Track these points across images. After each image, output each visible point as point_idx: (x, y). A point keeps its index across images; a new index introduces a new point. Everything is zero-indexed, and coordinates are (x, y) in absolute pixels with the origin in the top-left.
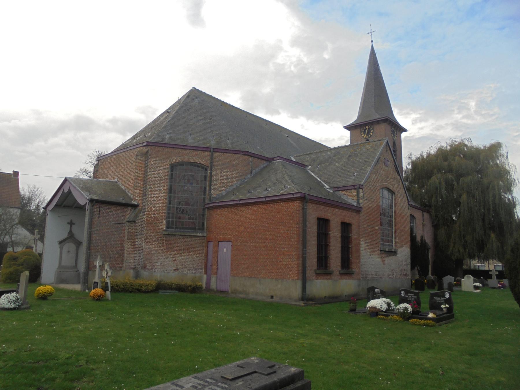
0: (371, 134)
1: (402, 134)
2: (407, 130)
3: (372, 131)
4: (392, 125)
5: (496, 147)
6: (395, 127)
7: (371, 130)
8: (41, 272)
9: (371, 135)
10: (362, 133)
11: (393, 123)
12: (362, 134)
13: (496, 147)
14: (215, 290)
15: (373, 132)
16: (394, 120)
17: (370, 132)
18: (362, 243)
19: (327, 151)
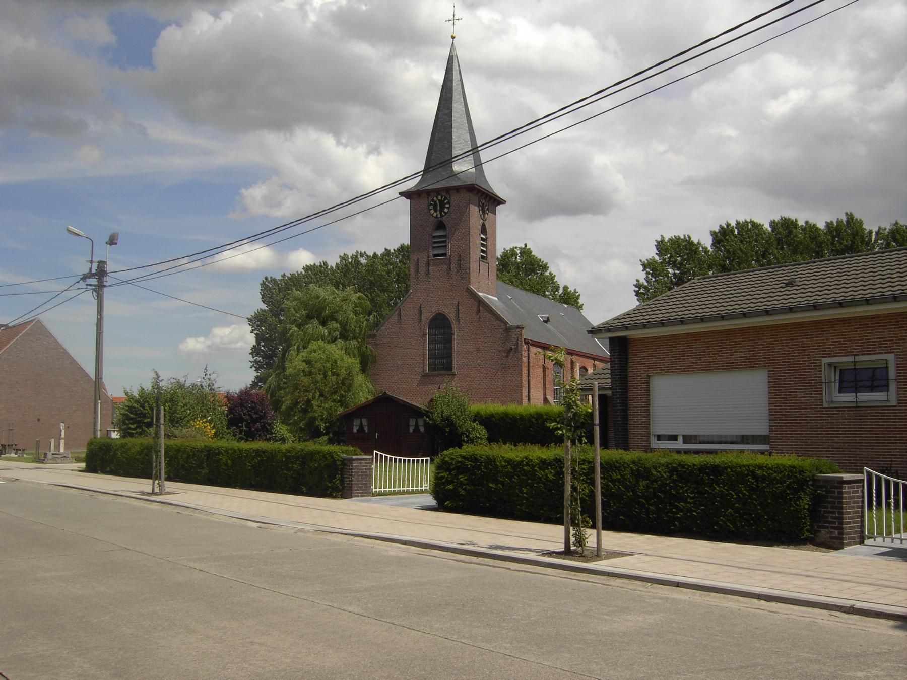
0: (446, 210)
1: (497, 208)
2: (506, 201)
3: (447, 206)
4: (490, 200)
5: (826, 222)
6: (485, 198)
7: (447, 203)
8: (595, 437)
9: (446, 213)
10: (431, 207)
11: (483, 193)
12: (431, 209)
13: (826, 222)
14: (124, 396)
15: (448, 208)
16: (491, 191)
17: (445, 207)
18: (412, 431)
19: (904, 557)
